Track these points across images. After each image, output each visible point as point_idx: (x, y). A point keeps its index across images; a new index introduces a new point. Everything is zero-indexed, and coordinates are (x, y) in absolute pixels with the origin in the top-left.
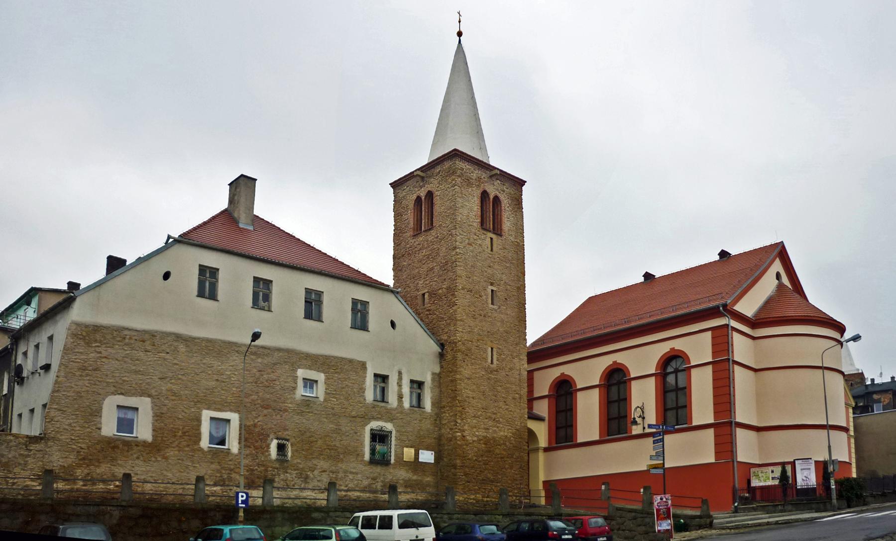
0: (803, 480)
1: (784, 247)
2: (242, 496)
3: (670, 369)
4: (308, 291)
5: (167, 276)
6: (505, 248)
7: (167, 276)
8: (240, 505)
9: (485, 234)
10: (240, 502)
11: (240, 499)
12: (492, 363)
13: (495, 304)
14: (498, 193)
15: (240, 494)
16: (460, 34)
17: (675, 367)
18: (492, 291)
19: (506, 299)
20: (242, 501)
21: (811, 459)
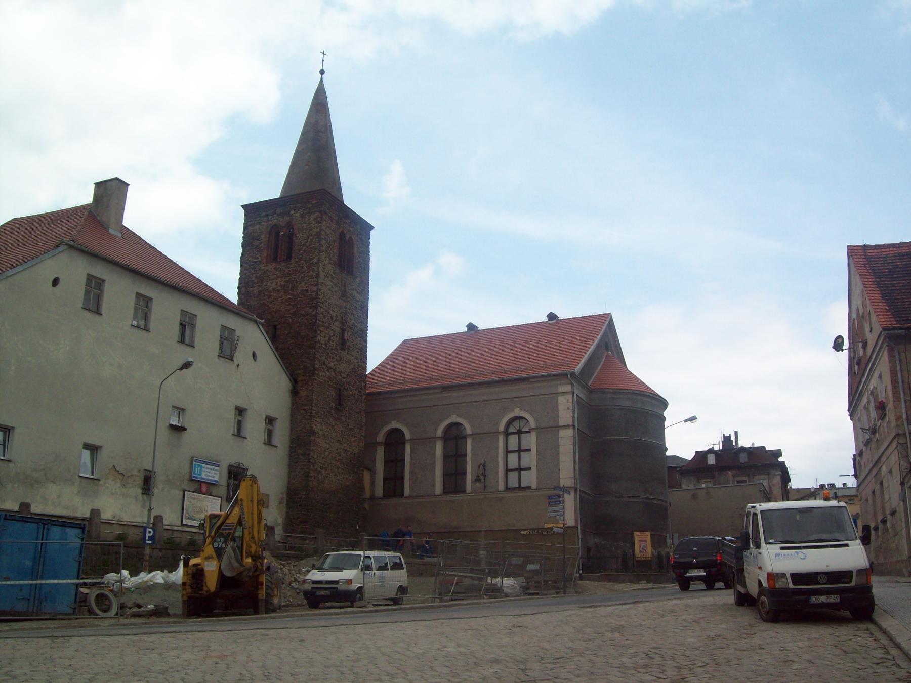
0: (641, 552)
1: (611, 326)
2: (150, 532)
3: (511, 430)
4: (184, 313)
5: (55, 282)
7: (55, 282)
8: (147, 542)
10: (147, 538)
11: (148, 535)
15: (148, 530)
16: (322, 72)
17: (518, 428)
20: (149, 536)
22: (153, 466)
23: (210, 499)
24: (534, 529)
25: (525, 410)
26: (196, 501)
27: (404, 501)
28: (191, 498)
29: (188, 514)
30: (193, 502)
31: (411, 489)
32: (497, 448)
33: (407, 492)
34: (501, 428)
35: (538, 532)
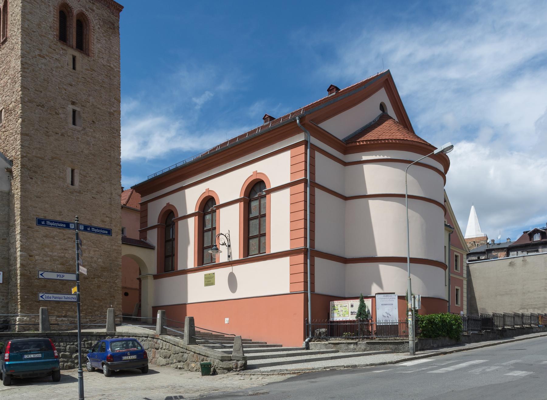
6: (93, 70)
9: (65, 50)
12: (72, 184)
13: (77, 125)
14: (84, 10)
18: (74, 112)
19: (93, 121)
21: (394, 293)
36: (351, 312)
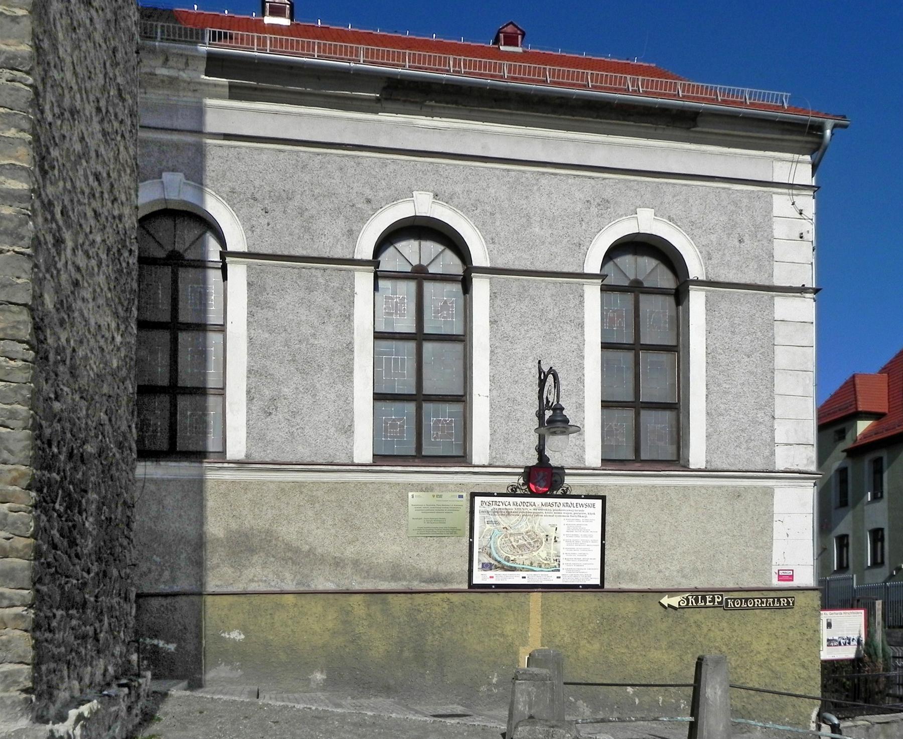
22: (420, 245)
23: (561, 508)
24: (696, 590)
25: (670, 219)
26: (514, 519)
27: (228, 476)
28: (494, 512)
29: (490, 555)
30: (503, 521)
31: (254, 435)
32: (581, 325)
33: (697, 455)
34: (365, 250)
35: (713, 600)
36: (828, 640)
